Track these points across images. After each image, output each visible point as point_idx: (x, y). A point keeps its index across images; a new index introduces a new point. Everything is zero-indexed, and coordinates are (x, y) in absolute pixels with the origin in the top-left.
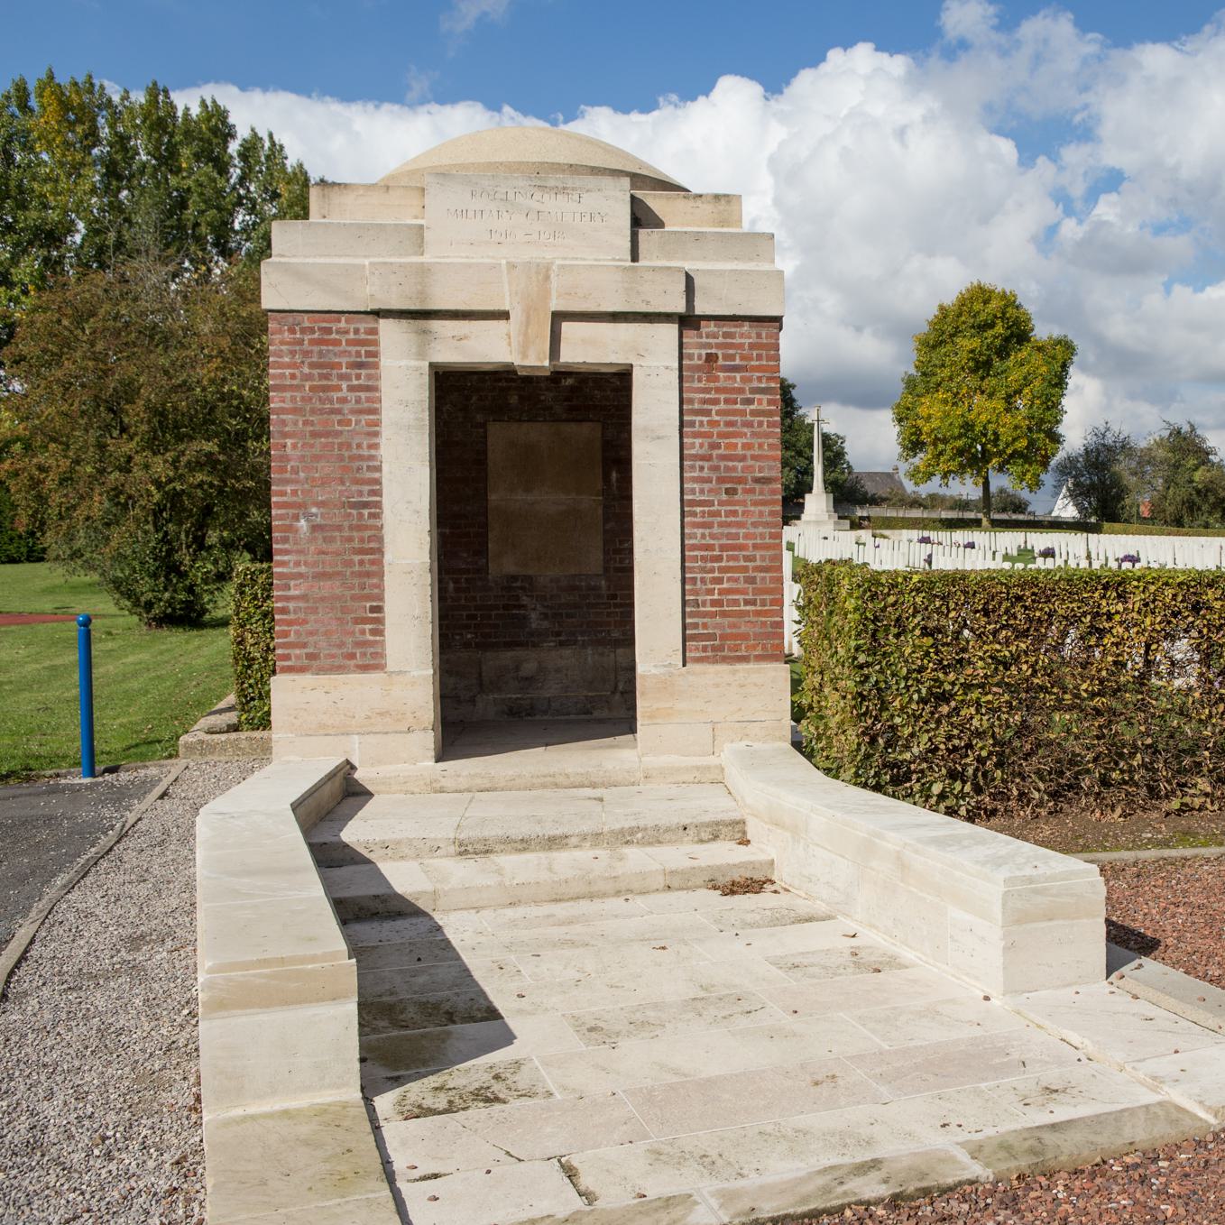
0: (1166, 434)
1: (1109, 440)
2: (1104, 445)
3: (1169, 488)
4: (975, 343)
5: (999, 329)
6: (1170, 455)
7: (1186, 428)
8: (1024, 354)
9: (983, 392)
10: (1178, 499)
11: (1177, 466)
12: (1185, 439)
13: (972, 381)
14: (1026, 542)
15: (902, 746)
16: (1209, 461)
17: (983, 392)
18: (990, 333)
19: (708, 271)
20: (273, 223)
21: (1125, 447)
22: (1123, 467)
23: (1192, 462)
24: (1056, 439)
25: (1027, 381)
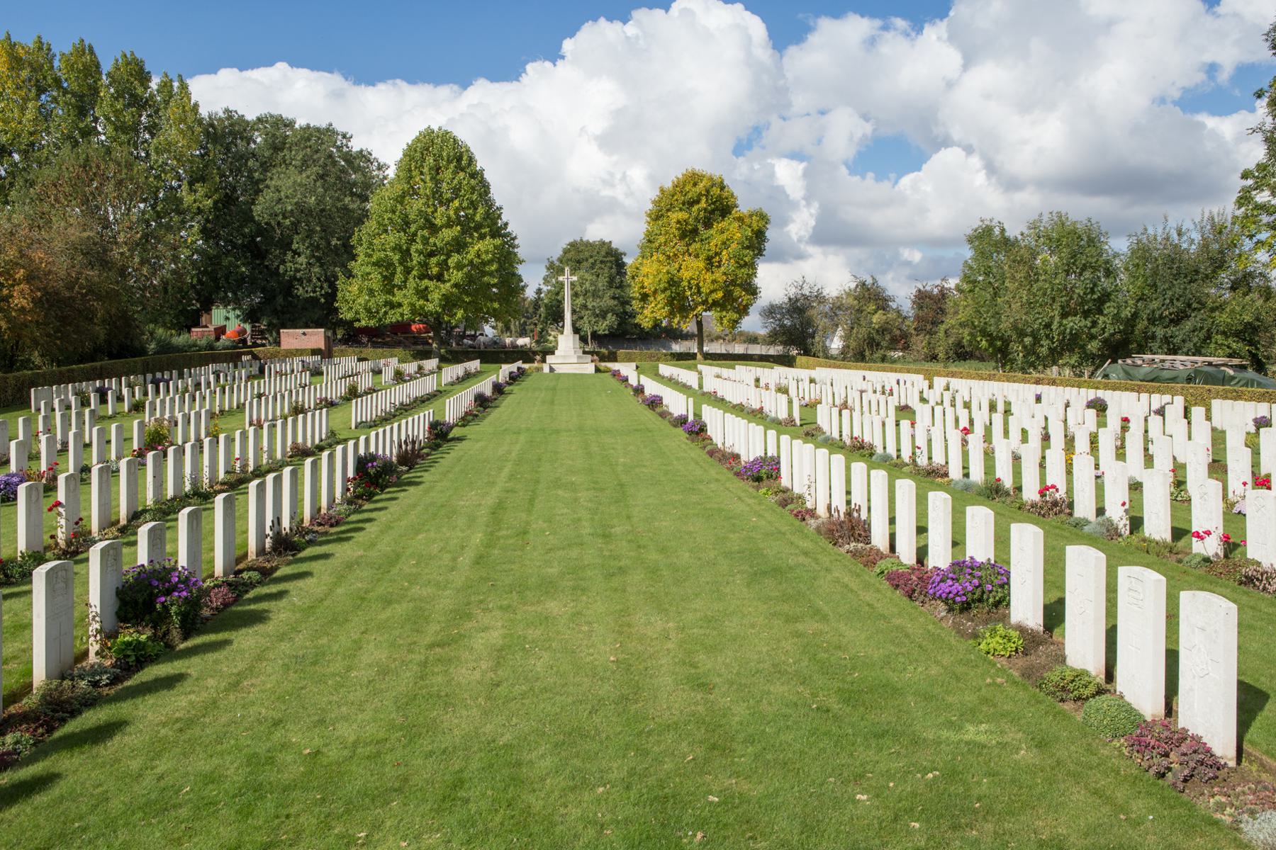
0: (853, 285)
1: (806, 292)
2: (803, 295)
3: (852, 328)
4: (682, 215)
5: (703, 204)
6: (856, 302)
7: (869, 281)
8: (723, 225)
9: (690, 255)
10: (860, 336)
11: (860, 311)
12: (868, 290)
13: (681, 247)
14: (899, 450)
15: (475, 283)
16: (888, 306)
17: (690, 255)
18: (695, 208)
19: (92, 359)
20: (1204, 409)
21: (820, 298)
22: (817, 314)
23: (872, 307)
24: (753, 291)
25: (725, 244)
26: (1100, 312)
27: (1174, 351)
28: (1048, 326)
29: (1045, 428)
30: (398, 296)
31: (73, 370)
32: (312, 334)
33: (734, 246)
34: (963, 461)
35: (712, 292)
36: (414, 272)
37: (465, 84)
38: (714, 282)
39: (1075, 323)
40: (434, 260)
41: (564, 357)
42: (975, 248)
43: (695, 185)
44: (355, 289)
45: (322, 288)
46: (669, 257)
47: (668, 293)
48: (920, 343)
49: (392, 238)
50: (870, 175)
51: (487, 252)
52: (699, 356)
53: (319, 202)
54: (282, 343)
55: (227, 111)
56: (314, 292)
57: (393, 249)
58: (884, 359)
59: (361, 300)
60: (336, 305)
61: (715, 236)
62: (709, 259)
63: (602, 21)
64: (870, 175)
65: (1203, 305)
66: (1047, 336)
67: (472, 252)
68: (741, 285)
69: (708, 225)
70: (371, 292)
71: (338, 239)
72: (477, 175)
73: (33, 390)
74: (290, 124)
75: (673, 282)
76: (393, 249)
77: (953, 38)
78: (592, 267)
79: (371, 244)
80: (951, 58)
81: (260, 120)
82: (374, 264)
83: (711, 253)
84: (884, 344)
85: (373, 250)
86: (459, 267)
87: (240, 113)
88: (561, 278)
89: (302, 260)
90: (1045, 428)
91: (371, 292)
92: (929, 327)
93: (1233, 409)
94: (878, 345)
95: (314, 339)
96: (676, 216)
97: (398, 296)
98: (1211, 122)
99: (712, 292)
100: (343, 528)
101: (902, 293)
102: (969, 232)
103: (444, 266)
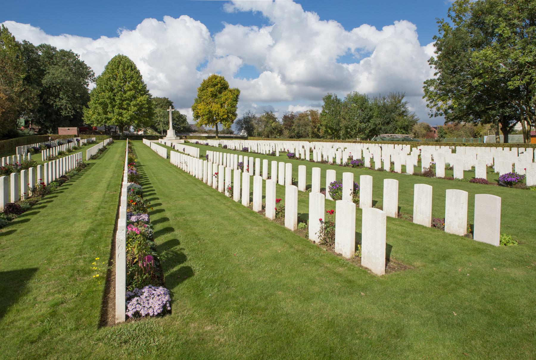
1: (250, 115)
5: (219, 85)
11: (267, 122)
18: (216, 87)
22: (254, 122)
23: (271, 121)
26: (369, 121)
27: (386, 133)
28: (355, 126)
29: (419, 156)
30: (110, 115)
31: (12, 141)
32: (72, 129)
33: (230, 100)
34: (260, 170)
35: (223, 115)
36: (116, 107)
37: (95, 37)
38: (224, 112)
39: (363, 125)
40: (125, 103)
41: (170, 138)
42: (326, 102)
43: (216, 79)
44: (91, 112)
45: (71, 112)
46: (207, 103)
47: (208, 115)
48: (286, 132)
49: (107, 94)
50: (245, 79)
51: (144, 100)
52: (216, 137)
53: (71, 79)
54: (59, 133)
55: (25, 41)
56: (68, 114)
57: (107, 98)
58: (275, 137)
59: (94, 116)
60: (83, 118)
61: (223, 96)
62: (221, 105)
63: (151, 19)
64: (245, 79)
65: (394, 120)
66: (355, 129)
67: (139, 100)
68: (232, 113)
69: (220, 92)
70: (99, 114)
71: (79, 94)
72: (138, 72)
73: (17, 147)
74: (54, 49)
75: (210, 112)
76: (107, 98)
77: (271, 34)
78: (162, 107)
79: (98, 96)
80: (269, 40)
81: (41, 46)
82: (99, 104)
83: (222, 102)
84: (275, 133)
85: (99, 98)
86: (134, 106)
87: (30, 42)
88: (168, 110)
89: (64, 101)
90: (419, 156)
91: (99, 114)
92: (289, 127)
93: (503, 150)
94: (273, 133)
95: (73, 131)
96: (210, 89)
97: (110, 115)
98: (345, 66)
99: (223, 115)
100: (52, 195)
101: (279, 117)
102: (324, 97)
103: (128, 105)
